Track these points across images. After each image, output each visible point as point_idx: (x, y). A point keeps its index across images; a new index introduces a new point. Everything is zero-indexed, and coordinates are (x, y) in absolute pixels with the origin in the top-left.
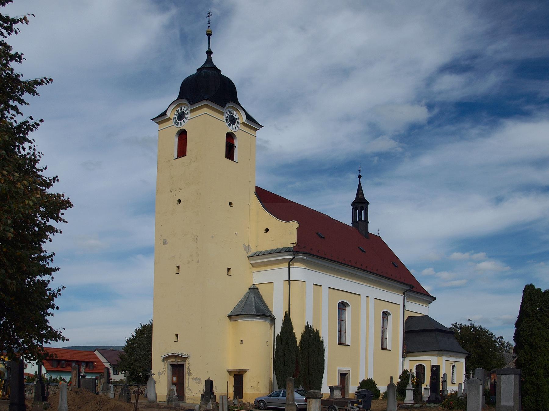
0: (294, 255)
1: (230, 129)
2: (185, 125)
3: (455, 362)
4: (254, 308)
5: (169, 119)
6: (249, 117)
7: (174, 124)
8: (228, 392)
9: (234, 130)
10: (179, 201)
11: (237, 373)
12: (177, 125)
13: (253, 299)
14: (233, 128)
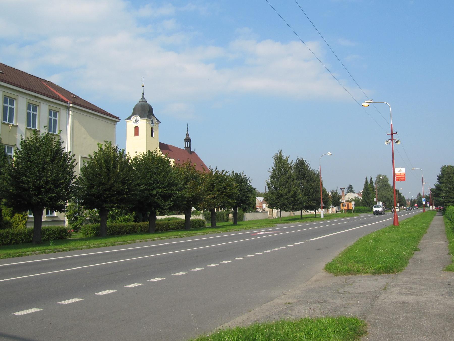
1: (152, 126)
5: (132, 121)
6: (157, 120)
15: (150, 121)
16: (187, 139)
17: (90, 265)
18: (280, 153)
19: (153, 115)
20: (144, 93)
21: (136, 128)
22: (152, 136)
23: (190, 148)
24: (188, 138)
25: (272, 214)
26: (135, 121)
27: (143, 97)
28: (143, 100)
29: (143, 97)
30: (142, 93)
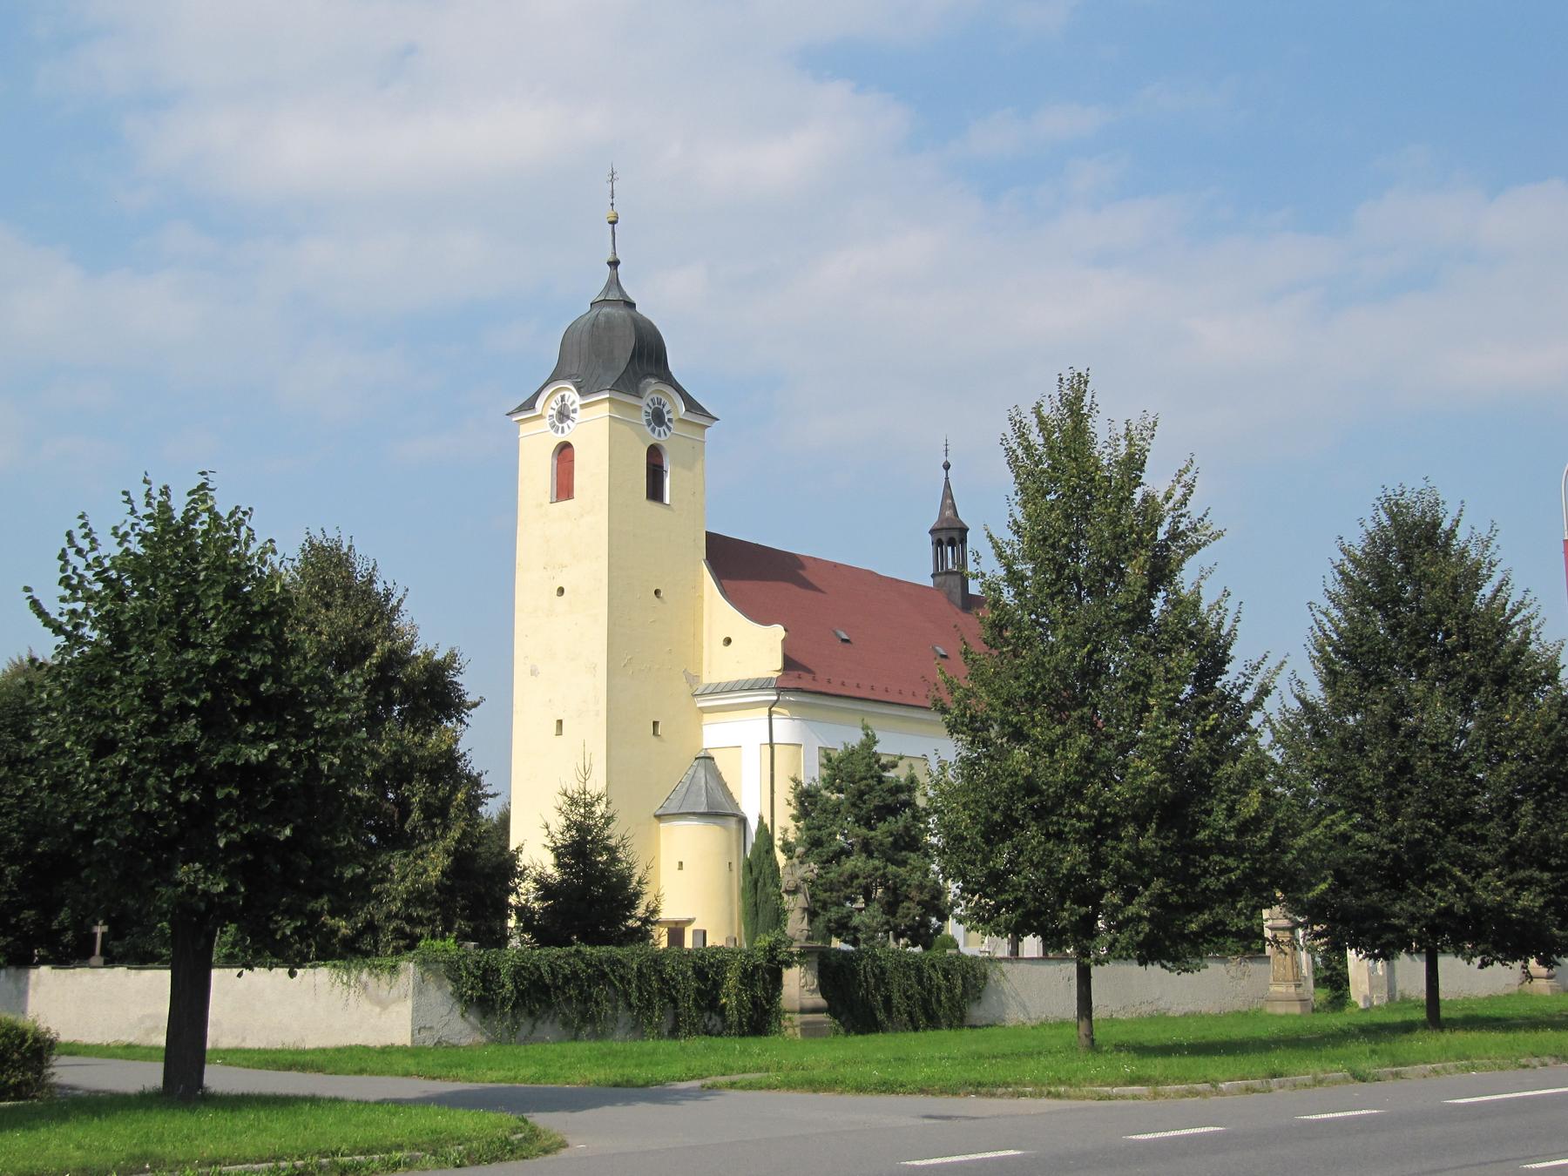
0: (779, 695)
1: (654, 439)
2: (570, 433)
4: (704, 799)
5: (540, 417)
6: (692, 405)
7: (549, 428)
9: (663, 437)
10: (561, 591)
11: (673, 926)
12: (557, 431)
14: (659, 435)
16: (945, 525)
17: (929, 1166)
18: (1074, 405)
19: (667, 379)
20: (619, 256)
21: (564, 451)
22: (655, 491)
23: (957, 579)
25: (1290, 975)
26: (554, 413)
27: (614, 282)
29: (614, 282)
30: (609, 257)
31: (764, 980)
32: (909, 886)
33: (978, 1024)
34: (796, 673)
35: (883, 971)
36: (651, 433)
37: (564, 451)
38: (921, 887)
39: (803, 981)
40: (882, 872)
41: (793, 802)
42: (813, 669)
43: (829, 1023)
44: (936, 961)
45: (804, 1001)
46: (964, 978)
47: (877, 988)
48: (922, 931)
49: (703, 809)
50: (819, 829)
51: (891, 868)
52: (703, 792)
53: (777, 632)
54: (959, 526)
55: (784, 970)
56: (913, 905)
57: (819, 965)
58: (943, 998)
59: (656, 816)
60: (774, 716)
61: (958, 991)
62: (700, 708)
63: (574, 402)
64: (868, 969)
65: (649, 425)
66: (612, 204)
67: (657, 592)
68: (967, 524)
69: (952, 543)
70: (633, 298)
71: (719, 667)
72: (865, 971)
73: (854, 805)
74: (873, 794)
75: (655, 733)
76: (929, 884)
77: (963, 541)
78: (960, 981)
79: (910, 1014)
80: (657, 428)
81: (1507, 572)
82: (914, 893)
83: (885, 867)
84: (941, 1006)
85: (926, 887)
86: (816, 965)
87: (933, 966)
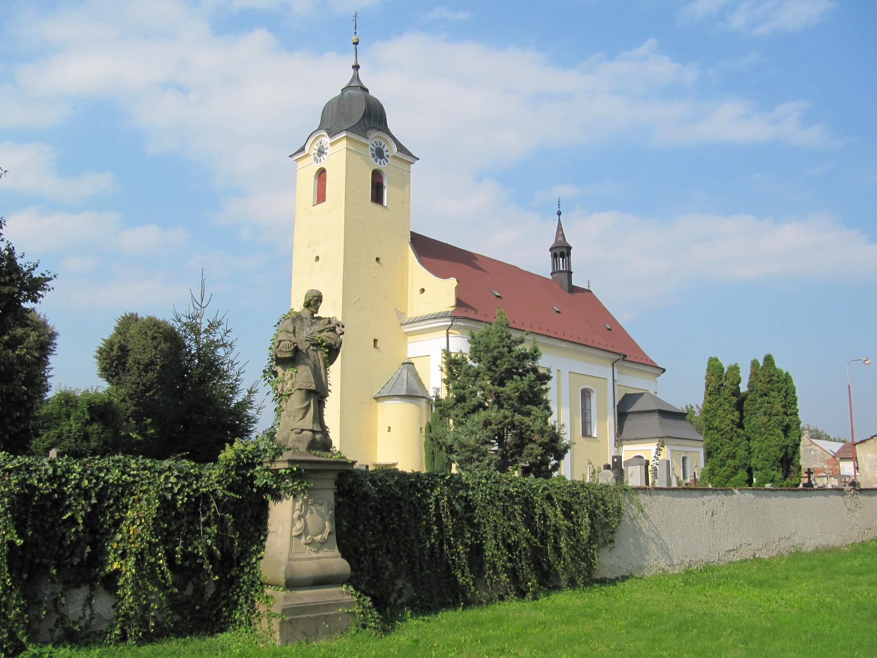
0: (452, 321)
1: (377, 166)
3: (686, 452)
4: (405, 387)
5: (308, 155)
6: (401, 148)
8: (661, 491)
10: (317, 258)
13: (406, 377)
15: (367, 146)
16: (558, 245)
21: (322, 173)
22: (377, 196)
23: (566, 275)
24: (560, 242)
27: (356, 77)
28: (357, 87)
29: (356, 77)
30: (353, 63)
31: (221, 522)
32: (532, 431)
33: (611, 576)
34: (465, 309)
35: (469, 507)
36: (374, 161)
37: (322, 173)
38: (542, 432)
39: (299, 525)
40: (510, 419)
41: (445, 370)
42: (476, 308)
43: (350, 604)
44: (552, 491)
45: (296, 564)
46: (592, 515)
47: (458, 534)
48: (543, 468)
49: (404, 393)
50: (463, 388)
51: (518, 417)
52: (405, 383)
53: (453, 282)
54: (566, 245)
55: (271, 504)
56: (536, 446)
57: (338, 495)
58: (563, 545)
59: (375, 398)
60: (450, 335)
61: (585, 534)
62: (405, 333)
63: (327, 143)
64: (444, 502)
65: (373, 157)
66: (355, 33)
67: (377, 259)
68: (571, 244)
69: (562, 255)
70: (366, 86)
71: (418, 307)
72: (437, 506)
73: (490, 369)
74: (504, 360)
75: (375, 346)
76: (549, 430)
77: (569, 254)
78: (587, 520)
79: (513, 574)
80: (379, 160)
81: (690, 405)
82: (536, 437)
83: (513, 416)
84: (559, 555)
85: (546, 432)
86: (330, 496)
87: (549, 498)
